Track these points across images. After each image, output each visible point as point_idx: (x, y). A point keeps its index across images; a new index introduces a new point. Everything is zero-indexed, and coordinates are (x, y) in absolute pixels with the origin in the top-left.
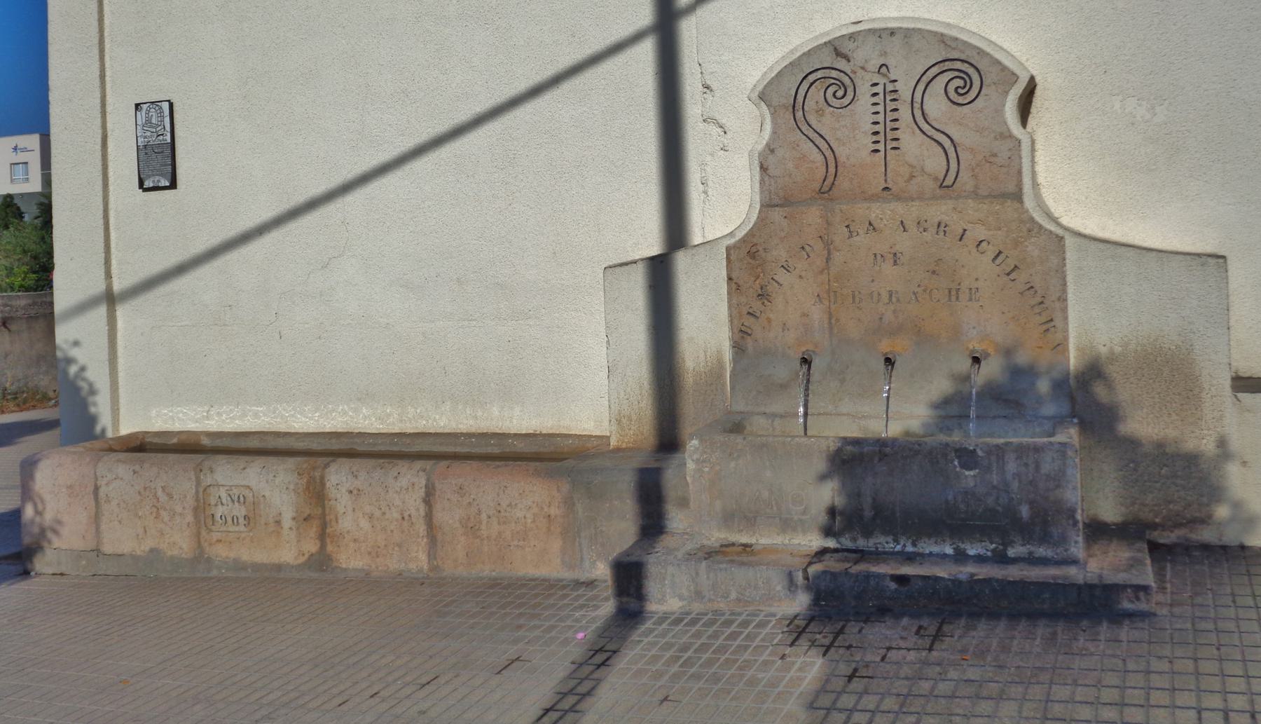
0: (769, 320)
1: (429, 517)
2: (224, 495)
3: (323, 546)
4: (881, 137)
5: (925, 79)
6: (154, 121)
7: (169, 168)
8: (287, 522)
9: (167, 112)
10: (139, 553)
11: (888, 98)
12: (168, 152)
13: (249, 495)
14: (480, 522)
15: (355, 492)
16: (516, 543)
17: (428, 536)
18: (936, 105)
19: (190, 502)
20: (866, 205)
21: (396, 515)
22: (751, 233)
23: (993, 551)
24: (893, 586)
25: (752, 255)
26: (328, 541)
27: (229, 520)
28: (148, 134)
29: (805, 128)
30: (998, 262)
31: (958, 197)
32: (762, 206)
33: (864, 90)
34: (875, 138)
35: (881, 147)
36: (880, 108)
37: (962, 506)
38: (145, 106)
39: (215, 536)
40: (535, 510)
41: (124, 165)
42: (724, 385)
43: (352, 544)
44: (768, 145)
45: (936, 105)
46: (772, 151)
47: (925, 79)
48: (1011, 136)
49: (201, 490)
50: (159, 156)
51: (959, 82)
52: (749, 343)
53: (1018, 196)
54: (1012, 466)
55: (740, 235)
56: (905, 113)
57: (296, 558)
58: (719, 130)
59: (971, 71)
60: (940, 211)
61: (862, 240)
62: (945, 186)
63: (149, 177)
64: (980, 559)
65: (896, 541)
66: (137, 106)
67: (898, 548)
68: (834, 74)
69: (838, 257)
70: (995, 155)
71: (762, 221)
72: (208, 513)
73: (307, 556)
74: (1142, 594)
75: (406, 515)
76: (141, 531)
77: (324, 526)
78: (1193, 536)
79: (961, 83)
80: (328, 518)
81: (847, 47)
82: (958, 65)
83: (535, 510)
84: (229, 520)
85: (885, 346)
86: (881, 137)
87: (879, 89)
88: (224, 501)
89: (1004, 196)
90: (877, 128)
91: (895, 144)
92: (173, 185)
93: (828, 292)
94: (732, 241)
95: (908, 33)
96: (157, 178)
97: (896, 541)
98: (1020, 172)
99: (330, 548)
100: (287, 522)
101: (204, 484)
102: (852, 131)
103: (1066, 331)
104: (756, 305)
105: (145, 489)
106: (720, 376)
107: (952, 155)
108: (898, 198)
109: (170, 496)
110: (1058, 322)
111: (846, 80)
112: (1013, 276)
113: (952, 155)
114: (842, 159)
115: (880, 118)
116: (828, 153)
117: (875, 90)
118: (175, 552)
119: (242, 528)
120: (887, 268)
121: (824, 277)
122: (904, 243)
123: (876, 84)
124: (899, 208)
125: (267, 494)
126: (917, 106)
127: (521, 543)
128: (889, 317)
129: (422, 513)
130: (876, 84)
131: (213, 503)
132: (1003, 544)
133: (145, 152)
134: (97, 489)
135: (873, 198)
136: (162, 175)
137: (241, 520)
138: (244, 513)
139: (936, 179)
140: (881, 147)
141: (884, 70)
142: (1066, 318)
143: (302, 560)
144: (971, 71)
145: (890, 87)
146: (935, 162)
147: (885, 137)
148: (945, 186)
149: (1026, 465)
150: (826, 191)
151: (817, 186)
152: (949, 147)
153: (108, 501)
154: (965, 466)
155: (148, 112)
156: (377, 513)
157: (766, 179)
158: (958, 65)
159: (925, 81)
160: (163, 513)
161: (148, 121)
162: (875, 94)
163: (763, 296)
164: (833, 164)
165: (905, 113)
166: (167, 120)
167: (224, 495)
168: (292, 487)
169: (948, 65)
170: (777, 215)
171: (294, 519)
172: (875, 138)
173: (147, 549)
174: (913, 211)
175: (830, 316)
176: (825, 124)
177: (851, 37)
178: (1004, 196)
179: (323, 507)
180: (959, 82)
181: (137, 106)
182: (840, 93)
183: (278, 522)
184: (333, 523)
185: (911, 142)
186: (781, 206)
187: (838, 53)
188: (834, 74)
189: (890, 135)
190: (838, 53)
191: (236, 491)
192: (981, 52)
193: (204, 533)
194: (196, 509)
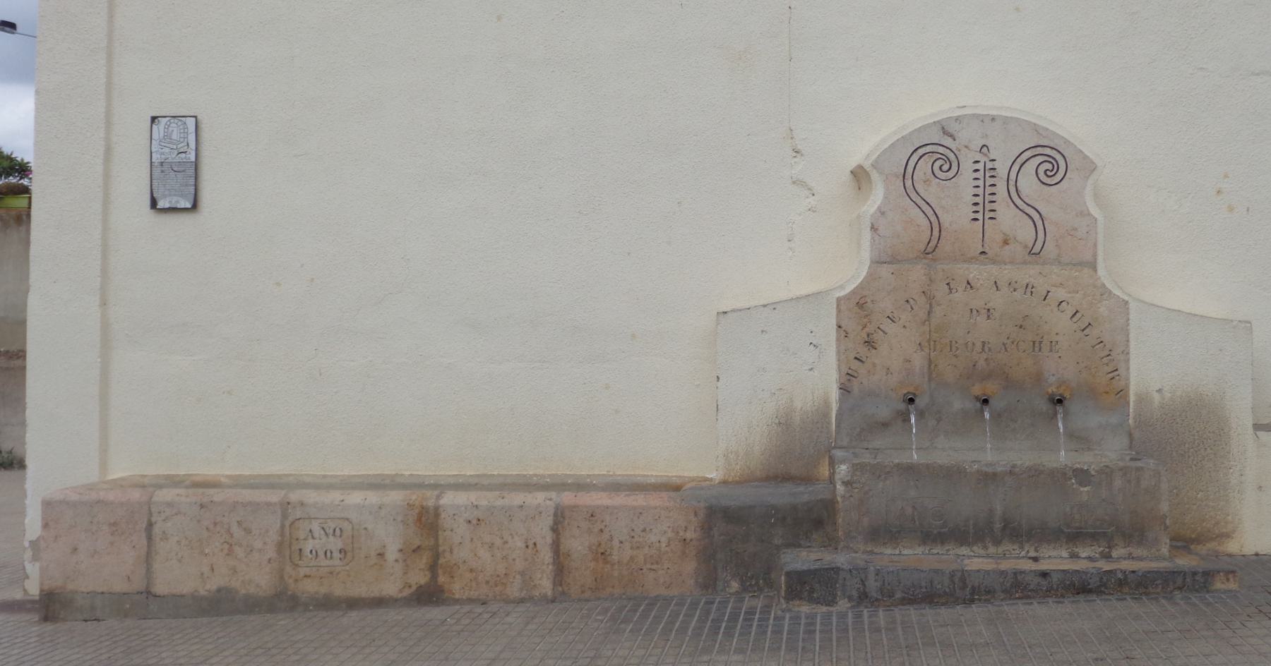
0: (874, 365)
1: (556, 546)
2: (316, 527)
3: (434, 576)
4: (980, 208)
5: (1020, 161)
6: (175, 136)
7: (192, 189)
8: (392, 554)
9: (192, 128)
10: (202, 592)
11: (988, 175)
12: (191, 172)
13: (346, 525)
14: (612, 548)
15: (475, 522)
16: (649, 566)
17: (554, 564)
18: (1028, 182)
19: (274, 536)
20: (966, 266)
21: (520, 544)
22: (861, 287)
23: (1101, 553)
24: (1038, 580)
25: (860, 305)
26: (440, 571)
27: (321, 554)
28: (167, 150)
29: (913, 195)
30: (1075, 319)
31: (1044, 263)
32: (872, 262)
33: (967, 166)
34: (975, 208)
35: (980, 216)
36: (981, 183)
37: (1077, 517)
38: (164, 121)
39: (303, 571)
40: (670, 534)
41: (132, 183)
42: (829, 423)
43: (468, 575)
44: (879, 208)
45: (1028, 182)
46: (883, 213)
47: (1020, 161)
48: (1089, 214)
49: (287, 524)
50: (180, 175)
51: (1049, 166)
52: (855, 382)
53: (1093, 266)
54: (1118, 483)
55: (850, 288)
56: (1001, 189)
57: (401, 591)
58: (807, 192)
59: (1058, 157)
60: (1029, 274)
61: (958, 296)
62: (1034, 253)
63: (165, 196)
64: (1090, 558)
65: (1022, 548)
66: (154, 119)
67: (1023, 553)
68: (941, 150)
69: (938, 311)
70: (1076, 229)
71: (871, 277)
72: (295, 547)
73: (414, 588)
74: (1230, 576)
75: (531, 544)
76: (206, 570)
77: (436, 556)
78: (1221, 549)
79: (1050, 167)
80: (441, 549)
81: (953, 127)
82: (1048, 151)
83: (670, 534)
84: (321, 554)
85: (977, 390)
86: (980, 208)
87: (980, 166)
88: (316, 535)
89: (1081, 264)
90: (977, 200)
91: (992, 214)
92: (195, 206)
93: (929, 341)
94: (842, 293)
95: (1006, 120)
96: (175, 199)
97: (1022, 548)
98: (1095, 245)
99: (442, 579)
100: (392, 554)
101: (291, 519)
102: (955, 200)
103: (1128, 379)
104: (863, 351)
105: (215, 524)
106: (826, 415)
107: (1039, 223)
108: (994, 262)
109: (248, 531)
110: (1122, 371)
111: (952, 156)
112: (1086, 332)
113: (1039, 223)
114: (945, 225)
115: (980, 191)
116: (933, 219)
117: (977, 166)
118: (252, 590)
119: (337, 562)
120: (981, 319)
121: (926, 328)
122: (998, 301)
123: (977, 162)
124: (994, 269)
125: (370, 527)
126: (1012, 183)
127: (654, 567)
128: (981, 363)
129: (549, 540)
130: (977, 162)
131: (302, 536)
132: (1109, 547)
133: (157, 170)
134: (150, 525)
135: (970, 260)
136: (182, 196)
137: (336, 555)
138: (340, 545)
139: (1026, 247)
140: (980, 216)
141: (985, 149)
142: (1128, 369)
143: (407, 592)
144: (1058, 157)
145: (990, 165)
146: (1025, 232)
147: (983, 208)
148: (1034, 253)
149: (1129, 481)
150: (929, 252)
151: (922, 247)
152: (1037, 220)
153: (165, 537)
154: (1081, 484)
155: (168, 126)
156: (498, 542)
157: (877, 238)
158: (1048, 151)
159: (1019, 162)
160: (236, 549)
161: (167, 136)
162: (977, 170)
163: (870, 343)
164: (936, 227)
165: (1001, 189)
166: (192, 138)
167: (316, 527)
168: (400, 518)
169: (1040, 150)
170: (885, 271)
171: (401, 550)
172: (975, 208)
173: (215, 588)
174: (1007, 273)
175: (930, 362)
176: (932, 192)
177: (957, 119)
178: (1081, 264)
179: (437, 539)
180: (1049, 166)
181: (154, 119)
182: (946, 167)
183: (381, 555)
184: (447, 554)
185: (1007, 217)
186: (889, 263)
187: (945, 132)
188: (941, 150)
189: (988, 206)
190: (945, 132)
191: (332, 525)
192: (1066, 142)
193: (288, 569)
194: (280, 546)
